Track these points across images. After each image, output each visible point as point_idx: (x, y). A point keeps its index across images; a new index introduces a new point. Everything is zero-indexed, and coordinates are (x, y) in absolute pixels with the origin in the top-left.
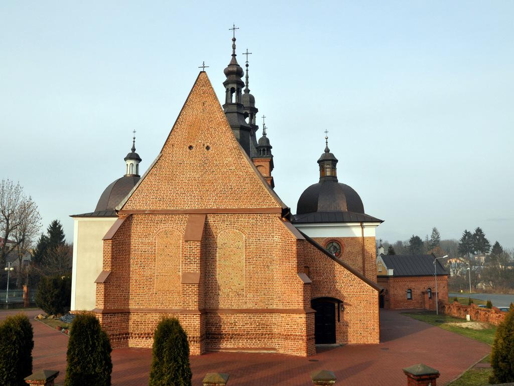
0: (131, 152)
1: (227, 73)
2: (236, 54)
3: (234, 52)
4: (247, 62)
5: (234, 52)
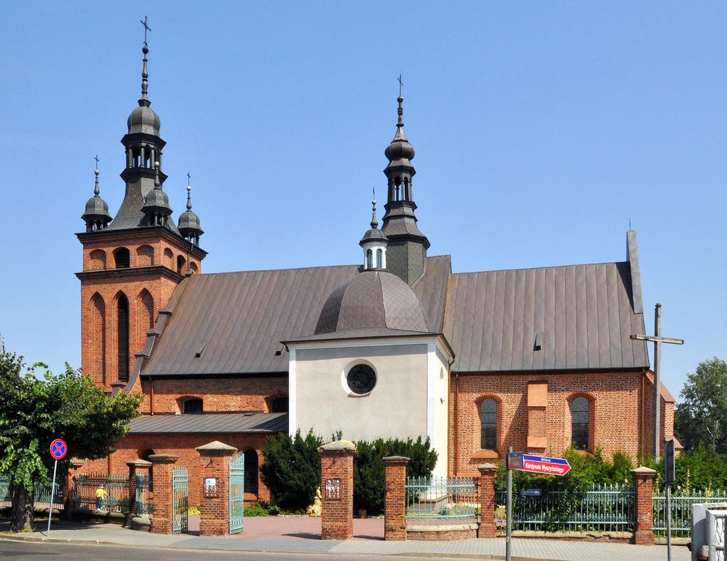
0: (370, 228)
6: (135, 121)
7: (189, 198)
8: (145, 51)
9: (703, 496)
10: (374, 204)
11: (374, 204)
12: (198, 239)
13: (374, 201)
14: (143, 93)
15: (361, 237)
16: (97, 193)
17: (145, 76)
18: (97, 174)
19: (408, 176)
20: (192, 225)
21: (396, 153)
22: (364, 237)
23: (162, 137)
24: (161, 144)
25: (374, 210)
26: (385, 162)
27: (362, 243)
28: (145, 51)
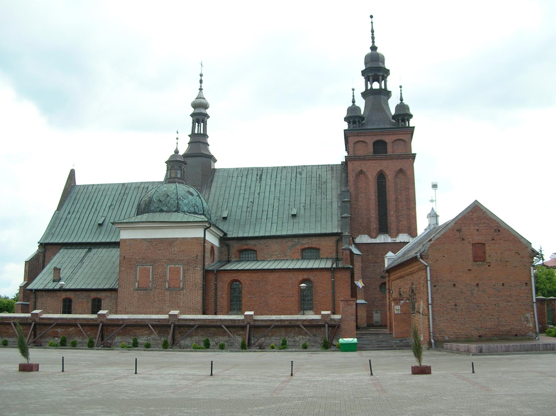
1: (195, 106)
2: (203, 88)
3: (201, 86)
5: (201, 86)
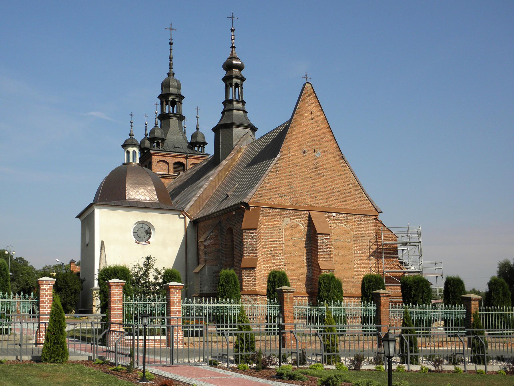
0: (129, 137)
4: (171, 39)
6: (165, 85)
7: (197, 123)
8: (171, 44)
9: (341, 305)
10: (131, 123)
11: (131, 123)
12: (204, 148)
13: (132, 121)
14: (170, 68)
15: (122, 144)
16: (197, 129)
17: (171, 59)
18: (197, 118)
19: (239, 81)
20: (199, 139)
21: (228, 66)
22: (124, 143)
23: (182, 93)
24: (181, 97)
25: (131, 126)
26: (224, 73)
27: (124, 146)
28: (171, 44)
